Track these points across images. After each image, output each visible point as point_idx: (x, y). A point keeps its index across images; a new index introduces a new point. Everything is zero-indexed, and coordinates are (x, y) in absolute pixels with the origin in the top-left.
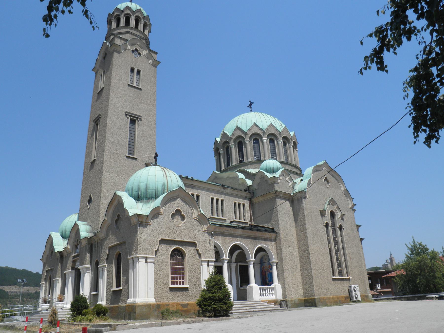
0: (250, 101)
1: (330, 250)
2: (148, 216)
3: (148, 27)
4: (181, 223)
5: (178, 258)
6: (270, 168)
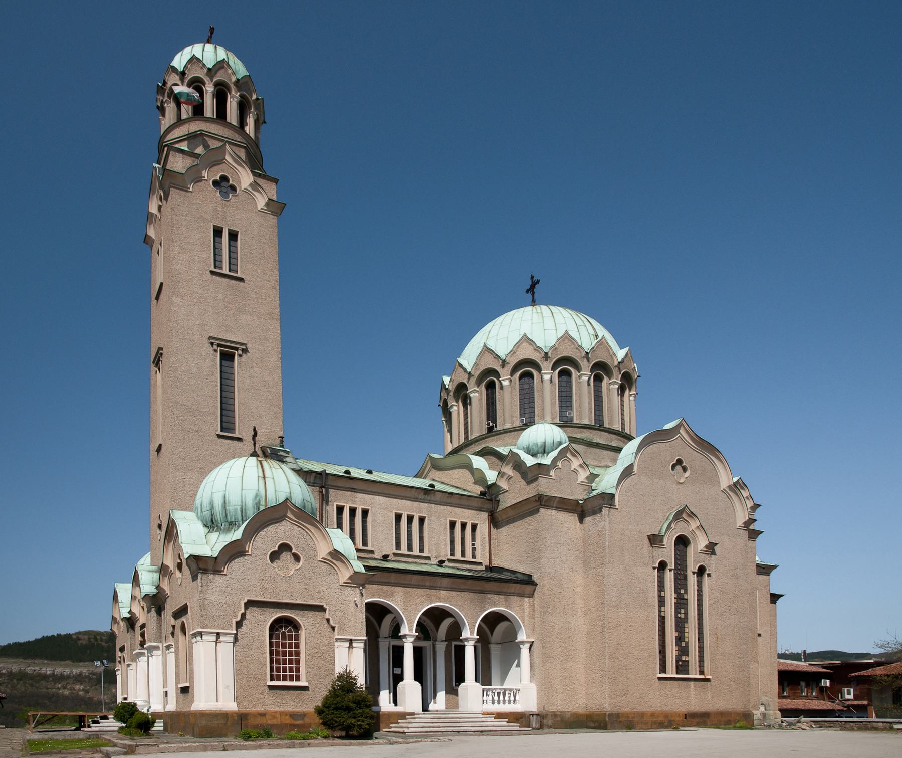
0: (532, 277)
1: (662, 620)
2: (216, 558)
3: (252, 110)
4: (293, 567)
5: (287, 633)
6: (537, 444)
